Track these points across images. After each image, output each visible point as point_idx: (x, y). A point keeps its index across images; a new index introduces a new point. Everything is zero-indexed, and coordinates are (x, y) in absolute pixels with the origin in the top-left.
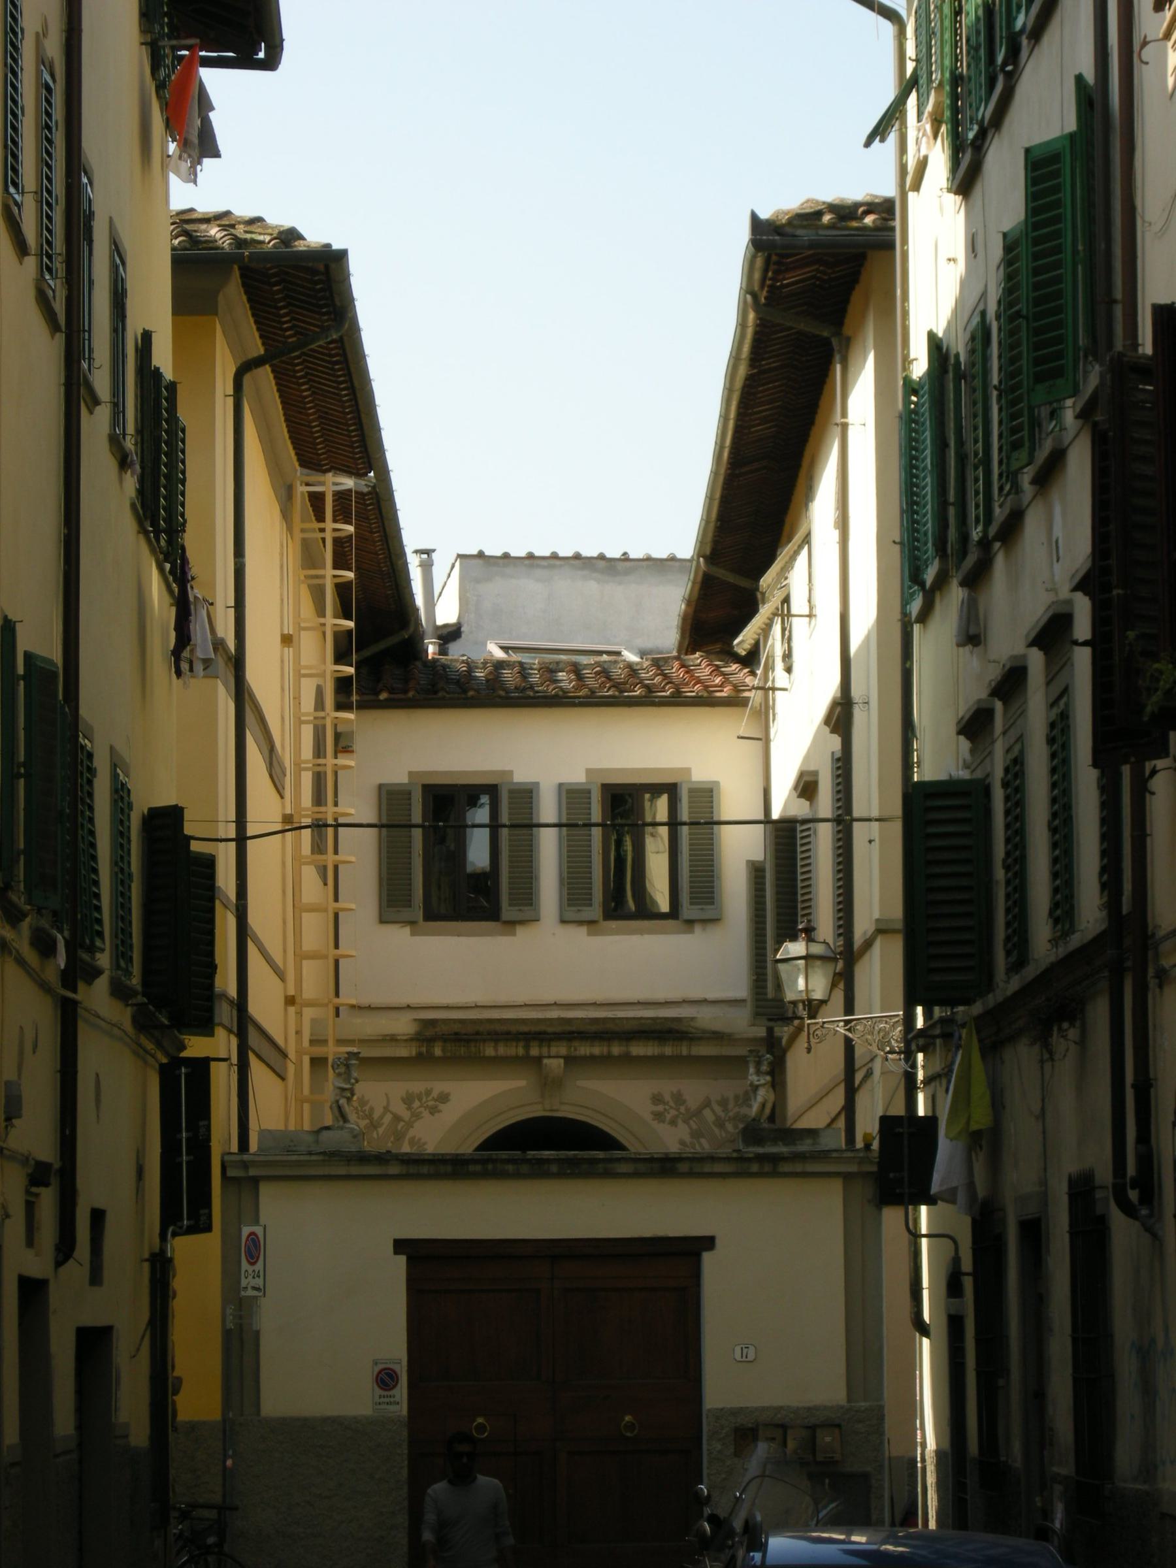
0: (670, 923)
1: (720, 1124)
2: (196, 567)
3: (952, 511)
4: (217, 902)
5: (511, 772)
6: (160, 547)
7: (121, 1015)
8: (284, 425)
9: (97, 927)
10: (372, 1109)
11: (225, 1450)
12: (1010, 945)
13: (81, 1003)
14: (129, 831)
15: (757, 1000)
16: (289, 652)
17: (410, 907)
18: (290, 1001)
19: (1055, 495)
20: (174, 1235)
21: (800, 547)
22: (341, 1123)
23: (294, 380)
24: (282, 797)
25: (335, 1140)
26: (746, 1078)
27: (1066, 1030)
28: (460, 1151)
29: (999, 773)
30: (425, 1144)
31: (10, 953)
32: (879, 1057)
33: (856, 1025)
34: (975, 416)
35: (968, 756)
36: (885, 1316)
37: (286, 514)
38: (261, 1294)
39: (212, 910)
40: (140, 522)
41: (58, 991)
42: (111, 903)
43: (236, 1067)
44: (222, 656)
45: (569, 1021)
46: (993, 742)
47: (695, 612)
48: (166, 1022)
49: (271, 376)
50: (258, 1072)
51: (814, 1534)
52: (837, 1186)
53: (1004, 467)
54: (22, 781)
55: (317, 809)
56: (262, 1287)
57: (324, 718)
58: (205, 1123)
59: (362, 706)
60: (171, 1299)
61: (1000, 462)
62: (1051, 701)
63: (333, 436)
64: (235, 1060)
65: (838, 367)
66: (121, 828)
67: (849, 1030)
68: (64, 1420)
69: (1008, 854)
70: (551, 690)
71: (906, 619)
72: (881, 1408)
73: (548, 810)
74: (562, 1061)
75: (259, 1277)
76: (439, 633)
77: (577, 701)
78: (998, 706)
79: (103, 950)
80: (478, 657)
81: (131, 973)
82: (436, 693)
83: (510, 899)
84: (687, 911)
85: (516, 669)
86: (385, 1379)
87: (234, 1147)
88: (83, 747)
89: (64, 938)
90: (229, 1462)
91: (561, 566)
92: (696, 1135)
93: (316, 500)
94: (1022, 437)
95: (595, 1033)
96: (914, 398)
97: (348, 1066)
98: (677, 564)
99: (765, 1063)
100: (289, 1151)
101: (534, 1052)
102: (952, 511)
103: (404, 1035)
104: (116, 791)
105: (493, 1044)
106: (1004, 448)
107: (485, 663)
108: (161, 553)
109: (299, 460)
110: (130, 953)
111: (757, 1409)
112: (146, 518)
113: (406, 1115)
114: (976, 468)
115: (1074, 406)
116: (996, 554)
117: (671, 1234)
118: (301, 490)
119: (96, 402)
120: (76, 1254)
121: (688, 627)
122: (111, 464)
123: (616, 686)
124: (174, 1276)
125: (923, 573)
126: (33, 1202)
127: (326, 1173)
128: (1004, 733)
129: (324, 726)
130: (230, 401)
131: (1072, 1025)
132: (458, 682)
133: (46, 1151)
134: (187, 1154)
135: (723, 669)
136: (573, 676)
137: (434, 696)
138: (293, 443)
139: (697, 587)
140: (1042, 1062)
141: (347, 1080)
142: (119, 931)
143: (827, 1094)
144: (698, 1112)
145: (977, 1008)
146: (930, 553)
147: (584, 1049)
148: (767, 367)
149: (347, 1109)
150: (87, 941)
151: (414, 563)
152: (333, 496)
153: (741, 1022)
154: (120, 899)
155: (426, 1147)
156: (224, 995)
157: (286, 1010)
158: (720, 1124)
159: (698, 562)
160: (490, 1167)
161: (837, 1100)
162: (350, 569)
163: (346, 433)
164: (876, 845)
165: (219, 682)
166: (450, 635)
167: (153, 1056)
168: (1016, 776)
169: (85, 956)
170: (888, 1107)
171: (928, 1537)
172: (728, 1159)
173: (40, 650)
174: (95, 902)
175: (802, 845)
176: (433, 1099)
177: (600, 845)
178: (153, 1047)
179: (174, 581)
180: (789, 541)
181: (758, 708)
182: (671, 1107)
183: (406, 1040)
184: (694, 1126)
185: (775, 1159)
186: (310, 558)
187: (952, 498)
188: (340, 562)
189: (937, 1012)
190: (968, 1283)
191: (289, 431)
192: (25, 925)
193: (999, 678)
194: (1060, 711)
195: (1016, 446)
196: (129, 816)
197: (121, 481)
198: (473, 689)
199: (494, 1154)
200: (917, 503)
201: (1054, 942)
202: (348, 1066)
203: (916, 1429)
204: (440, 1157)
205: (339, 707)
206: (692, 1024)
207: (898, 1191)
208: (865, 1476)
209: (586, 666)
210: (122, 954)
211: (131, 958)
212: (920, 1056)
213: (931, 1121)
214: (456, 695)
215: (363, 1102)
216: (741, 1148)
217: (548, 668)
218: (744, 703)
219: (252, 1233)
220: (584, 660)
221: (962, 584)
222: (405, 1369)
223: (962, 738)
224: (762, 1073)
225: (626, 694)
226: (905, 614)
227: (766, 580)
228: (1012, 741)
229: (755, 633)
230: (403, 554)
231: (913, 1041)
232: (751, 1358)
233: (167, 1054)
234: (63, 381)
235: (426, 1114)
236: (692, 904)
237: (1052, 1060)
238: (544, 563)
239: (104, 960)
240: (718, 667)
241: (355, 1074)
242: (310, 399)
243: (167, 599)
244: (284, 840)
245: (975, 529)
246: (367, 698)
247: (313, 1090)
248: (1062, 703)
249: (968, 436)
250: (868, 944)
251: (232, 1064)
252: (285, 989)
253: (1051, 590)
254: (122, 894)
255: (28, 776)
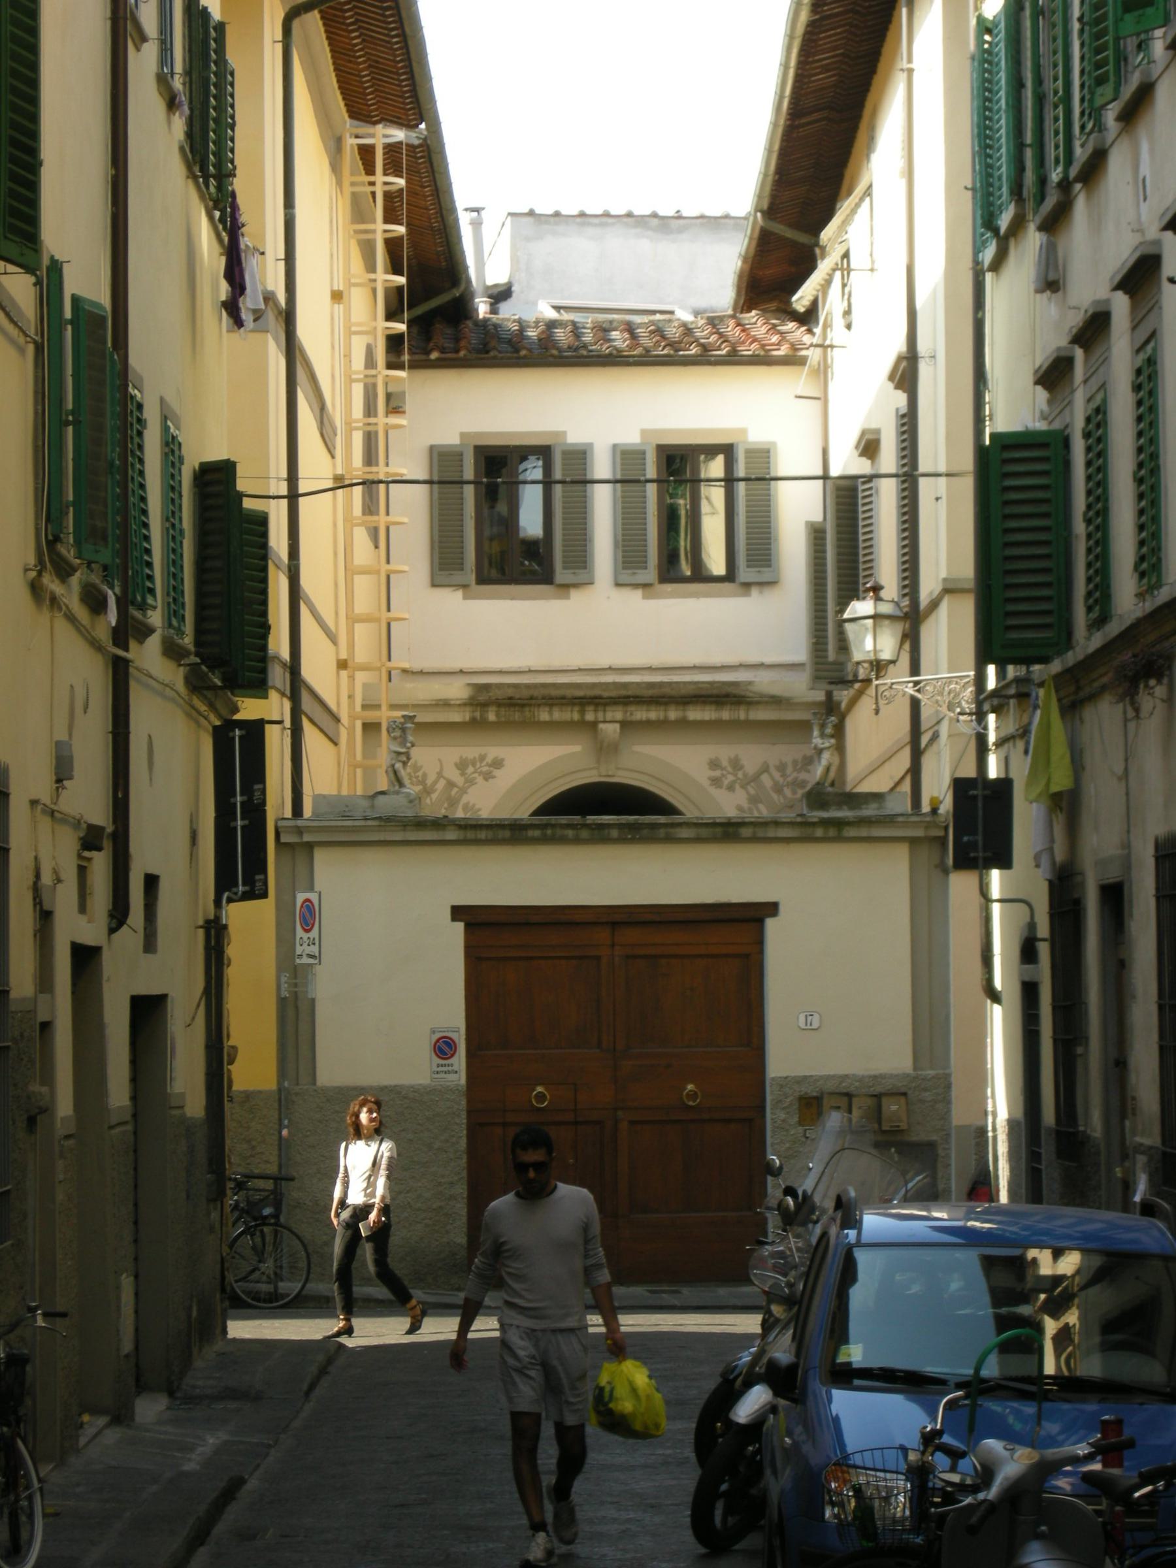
0: (727, 586)
1: (778, 789)
2: (246, 215)
3: (1029, 154)
4: (270, 562)
5: (565, 433)
6: (209, 194)
7: (173, 675)
8: (333, 74)
9: (149, 584)
10: (425, 775)
11: (280, 1120)
12: (1091, 601)
13: (132, 661)
14: (180, 486)
15: (817, 663)
16: (339, 309)
17: (462, 569)
18: (342, 665)
19: (1142, 132)
20: (230, 900)
21: (862, 200)
22: (397, 788)
23: (344, 27)
24: (333, 457)
25: (389, 805)
26: (811, 743)
27: (1152, 688)
28: (515, 816)
29: (1079, 424)
30: (479, 810)
31: (60, 609)
32: (947, 718)
33: (925, 686)
34: (1055, 53)
35: (1045, 407)
36: (952, 982)
37: (335, 167)
38: (317, 961)
39: (265, 569)
40: (189, 168)
41: (109, 649)
42: (162, 559)
43: (289, 731)
44: (272, 310)
45: (625, 685)
46: (1073, 391)
47: (752, 269)
48: (219, 684)
49: (320, 23)
50: (311, 737)
51: (894, 1211)
52: (902, 853)
53: (1086, 104)
54: (70, 429)
55: (368, 469)
56: (317, 955)
57: (375, 376)
58: (260, 786)
59: (414, 366)
60: (225, 967)
61: (1082, 100)
62: (1138, 345)
63: (384, 87)
64: (288, 724)
65: (904, 11)
66: (172, 482)
67: (918, 691)
68: (119, 1093)
69: (1089, 507)
70: (605, 349)
71: (979, 267)
72: (948, 1076)
73: (602, 467)
74: (617, 726)
75: (314, 944)
76: (490, 292)
77: (631, 360)
78: (1079, 353)
79: (155, 608)
80: (529, 317)
81: (183, 633)
82: (487, 352)
83: (564, 562)
84: (745, 573)
85: (569, 328)
86: (443, 1048)
87: (288, 813)
88: (132, 397)
89: (115, 594)
90: (285, 1132)
91: (613, 224)
92: (754, 800)
93: (366, 153)
94: (1108, 71)
95: (651, 697)
96: (987, 38)
97: (403, 730)
98: (732, 222)
99: (830, 725)
100: (346, 817)
101: (590, 716)
102: (1029, 154)
103: (457, 699)
104: (167, 444)
105: (547, 709)
106: (1087, 84)
107: (537, 322)
108: (211, 200)
109: (348, 111)
110: (182, 612)
111: (821, 1077)
112: (195, 163)
113: (459, 780)
114: (1056, 107)
115: (1164, 37)
116: (1076, 196)
117: (734, 900)
118: (351, 142)
119: (144, 38)
120: (130, 921)
121: (744, 285)
122: (160, 105)
123: (671, 345)
124: (228, 944)
125: (997, 220)
126: (85, 867)
127: (382, 839)
128: (1085, 381)
129: (375, 385)
130: (279, 47)
131: (1159, 682)
132: (509, 342)
133: (99, 814)
134: (242, 819)
135: (779, 328)
136: (626, 335)
137: (486, 356)
138: (342, 93)
139: (754, 243)
140: (1126, 721)
141: (403, 744)
142: (171, 590)
143: (890, 757)
144: (756, 778)
145: (1056, 666)
146: (1004, 198)
147: (640, 714)
148: (829, 13)
149: (403, 773)
150: (139, 598)
151: (464, 221)
152: (384, 148)
153: (800, 687)
154: (172, 556)
155: (479, 813)
156: (277, 658)
157: (338, 674)
158: (778, 789)
159: (755, 217)
160: (549, 832)
161: (904, 760)
162: (401, 224)
163: (396, 82)
164: (943, 502)
165: (269, 336)
166: (501, 295)
167: (206, 718)
168: (1098, 426)
169: (137, 614)
170: (956, 768)
171: (1002, 1211)
172: (791, 824)
173: (85, 293)
174: (146, 558)
175: (864, 505)
176: (488, 765)
177: (655, 507)
178: (206, 708)
179: (225, 228)
180: (849, 193)
181: (816, 367)
182: (729, 773)
183: (460, 705)
184: (752, 791)
185: (840, 824)
186: (359, 213)
187: (1029, 138)
188: (390, 217)
189: (1011, 671)
190: (1044, 950)
191: (338, 81)
192: (75, 580)
193: (1081, 324)
194: (1146, 356)
195: (1101, 81)
196: (180, 470)
197: (169, 122)
198: (525, 348)
199: (553, 819)
200: (990, 147)
201: (1140, 596)
202: (403, 730)
203: (987, 1098)
204: (498, 822)
205: (390, 366)
206: (750, 688)
207: (972, 855)
208: (932, 1145)
209: (640, 325)
210: (174, 612)
211: (183, 617)
212: (992, 718)
213: (1004, 786)
214: (509, 355)
215: (416, 768)
216: (805, 812)
217: (601, 327)
218: (802, 362)
219: (308, 900)
220: (637, 319)
221: (1042, 228)
222: (463, 1037)
223: (1039, 388)
224: (826, 735)
225: (681, 353)
226: (977, 263)
227: (826, 234)
228: (1094, 389)
229: (814, 289)
230: (453, 210)
231: (985, 702)
232: (814, 1027)
233: (220, 716)
234: (109, 14)
235: (480, 779)
236: (748, 566)
237: (1137, 717)
238: (596, 221)
239: (155, 618)
240: (774, 326)
241: (410, 738)
242: (360, 47)
243: (217, 249)
244: (335, 498)
245: (1055, 170)
246: (417, 357)
247: (365, 755)
248: (1149, 348)
249: (1047, 74)
250: (934, 605)
251: (284, 728)
252: (337, 653)
253: (1138, 231)
254: (174, 551)
255: (76, 423)
